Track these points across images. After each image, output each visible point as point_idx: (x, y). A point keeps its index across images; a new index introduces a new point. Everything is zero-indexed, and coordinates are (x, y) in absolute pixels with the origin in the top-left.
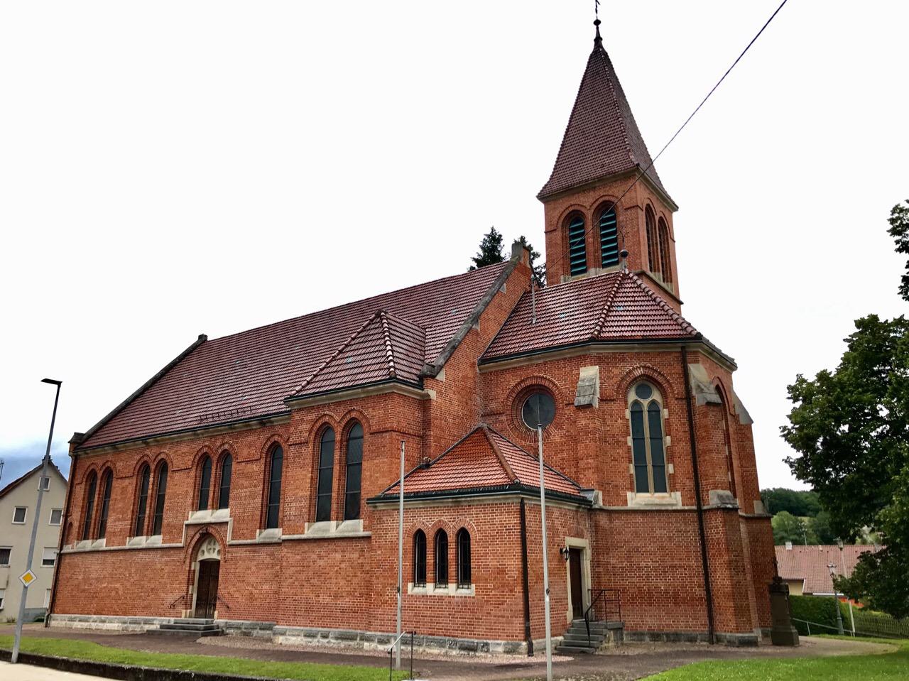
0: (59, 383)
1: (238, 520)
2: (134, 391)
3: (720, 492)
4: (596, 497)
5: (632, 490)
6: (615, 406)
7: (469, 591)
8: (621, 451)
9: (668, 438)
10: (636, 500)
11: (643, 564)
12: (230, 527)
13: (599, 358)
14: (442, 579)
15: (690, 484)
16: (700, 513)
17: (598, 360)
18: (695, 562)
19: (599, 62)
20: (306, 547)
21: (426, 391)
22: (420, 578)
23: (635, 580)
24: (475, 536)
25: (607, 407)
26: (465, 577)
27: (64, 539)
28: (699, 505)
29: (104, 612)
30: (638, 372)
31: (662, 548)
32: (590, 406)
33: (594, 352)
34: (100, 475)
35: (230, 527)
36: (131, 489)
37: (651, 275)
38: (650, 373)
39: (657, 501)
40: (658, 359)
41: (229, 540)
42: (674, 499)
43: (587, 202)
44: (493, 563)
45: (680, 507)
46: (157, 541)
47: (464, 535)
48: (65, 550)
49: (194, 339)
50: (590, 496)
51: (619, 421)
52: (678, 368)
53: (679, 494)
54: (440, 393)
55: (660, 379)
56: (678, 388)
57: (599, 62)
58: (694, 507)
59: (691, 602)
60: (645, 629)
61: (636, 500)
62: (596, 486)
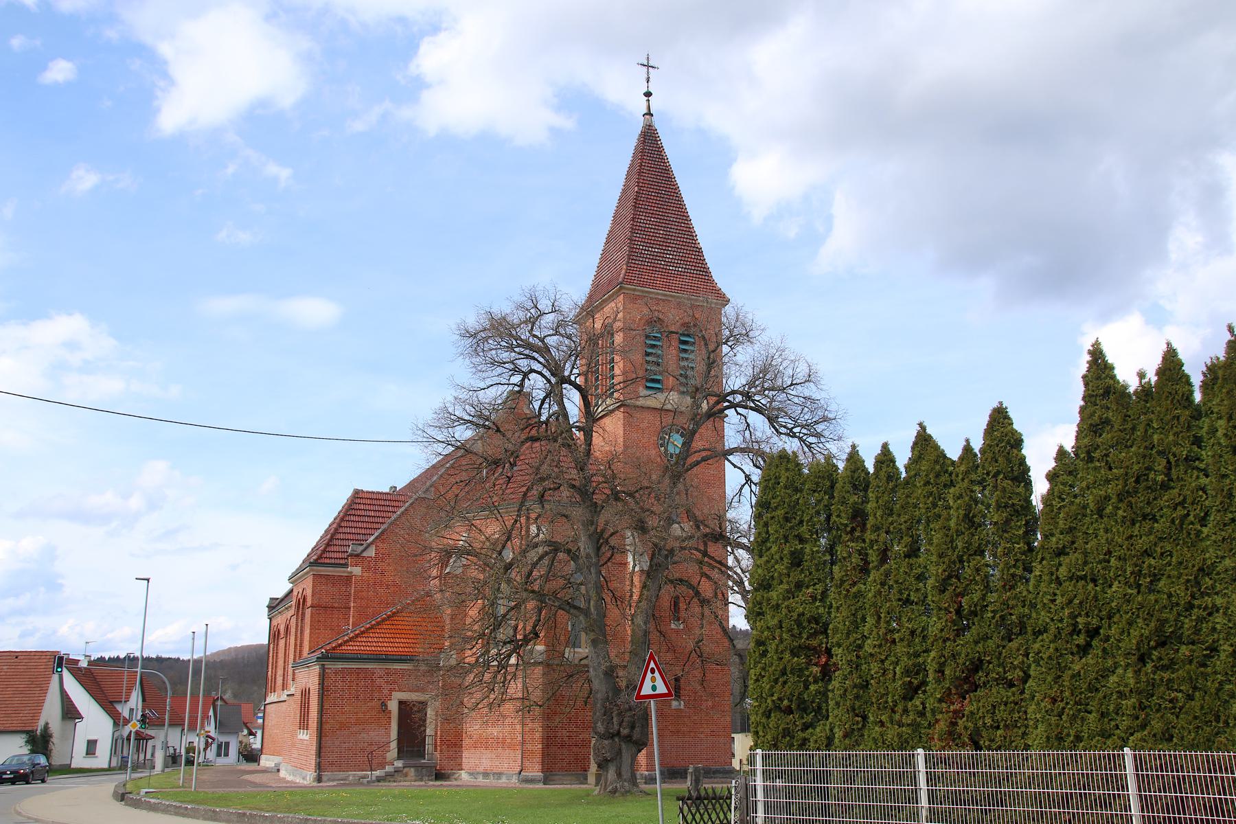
0: (148, 580)
59: (511, 747)
60: (481, 769)
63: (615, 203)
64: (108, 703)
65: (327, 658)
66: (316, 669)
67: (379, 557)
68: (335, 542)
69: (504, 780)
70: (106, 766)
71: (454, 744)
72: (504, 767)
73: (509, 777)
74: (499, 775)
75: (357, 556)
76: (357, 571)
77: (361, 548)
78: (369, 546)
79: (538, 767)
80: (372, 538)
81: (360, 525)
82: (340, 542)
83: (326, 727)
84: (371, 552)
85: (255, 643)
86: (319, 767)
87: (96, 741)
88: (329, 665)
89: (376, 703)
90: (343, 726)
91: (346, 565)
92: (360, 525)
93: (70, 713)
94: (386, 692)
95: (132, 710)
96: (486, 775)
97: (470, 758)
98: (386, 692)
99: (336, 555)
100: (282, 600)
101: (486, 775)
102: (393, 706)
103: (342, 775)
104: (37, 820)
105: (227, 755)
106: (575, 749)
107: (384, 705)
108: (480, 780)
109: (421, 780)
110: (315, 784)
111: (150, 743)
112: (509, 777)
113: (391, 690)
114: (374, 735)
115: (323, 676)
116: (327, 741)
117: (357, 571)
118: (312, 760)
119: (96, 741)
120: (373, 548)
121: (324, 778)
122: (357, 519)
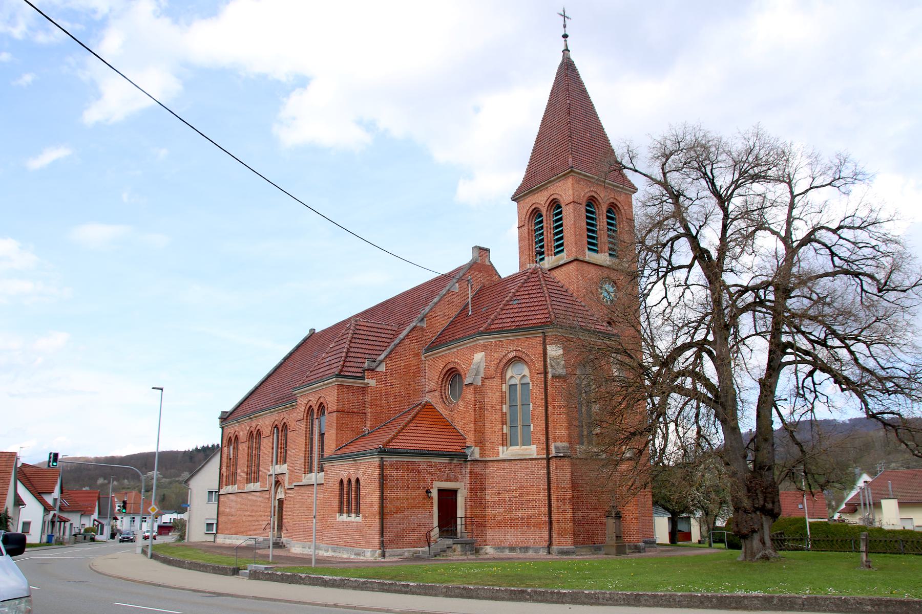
0: (162, 389)
1: (292, 471)
2: (78, 456)
3: (559, 444)
4: (473, 453)
5: (503, 445)
6: (497, 381)
7: (359, 519)
8: (496, 416)
9: (504, 410)
10: (505, 452)
11: (507, 499)
12: (287, 476)
13: (485, 346)
14: (349, 512)
15: (543, 438)
16: (548, 459)
17: (485, 348)
18: (543, 497)
19: (568, 70)
20: (303, 489)
21: (366, 381)
22: (341, 512)
23: (502, 510)
24: (362, 482)
25: (487, 383)
26: (358, 512)
27: (220, 486)
28: (548, 454)
29: (646, 598)
30: (511, 355)
31: (521, 487)
32: (471, 384)
33: (481, 342)
34: (316, 411)
35: (287, 476)
36: (246, 449)
37: (590, 256)
38: (520, 354)
39: (521, 452)
40: (526, 344)
41: (287, 486)
42: (533, 450)
43: (541, 199)
44: (368, 501)
45: (535, 456)
46: (256, 486)
47: (358, 480)
48: (222, 492)
49: (306, 333)
50: (468, 452)
51: (497, 394)
52: (540, 349)
53: (535, 446)
54: (380, 381)
55: (526, 359)
56: (540, 366)
57: (568, 70)
58: (545, 456)
59: (538, 526)
60: (507, 544)
61: (505, 452)
62: (473, 445)
63: (586, 86)
64: (38, 495)
65: (385, 452)
66: (376, 460)
67: (389, 373)
68: (349, 359)
69: (530, 553)
70: (38, 542)
71: (478, 522)
72: (531, 542)
73: (536, 551)
74: (526, 549)
75: (373, 370)
76: (372, 382)
77: (375, 364)
78: (381, 362)
79: (570, 541)
80: (382, 357)
81: (364, 346)
82: (352, 359)
83: (386, 511)
84: (382, 368)
85: (136, 453)
86: (382, 545)
87: (29, 523)
88: (389, 459)
89: (422, 491)
90: (398, 510)
91: (363, 378)
92: (364, 346)
93: (19, 502)
94: (429, 481)
95: (55, 500)
96: (512, 549)
97: (493, 536)
98: (429, 481)
99: (351, 369)
100: (232, 413)
101: (512, 549)
102: (435, 494)
103: (399, 551)
104: (388, 611)
105: (102, 533)
106: (587, 526)
107: (428, 492)
108: (507, 554)
109: (466, 554)
110: (380, 559)
111: (68, 524)
112: (536, 551)
113: (432, 480)
114: (421, 517)
115: (382, 468)
116: (387, 523)
117: (372, 382)
118: (376, 540)
119: (29, 523)
120: (384, 364)
121: (387, 554)
122: (360, 341)
